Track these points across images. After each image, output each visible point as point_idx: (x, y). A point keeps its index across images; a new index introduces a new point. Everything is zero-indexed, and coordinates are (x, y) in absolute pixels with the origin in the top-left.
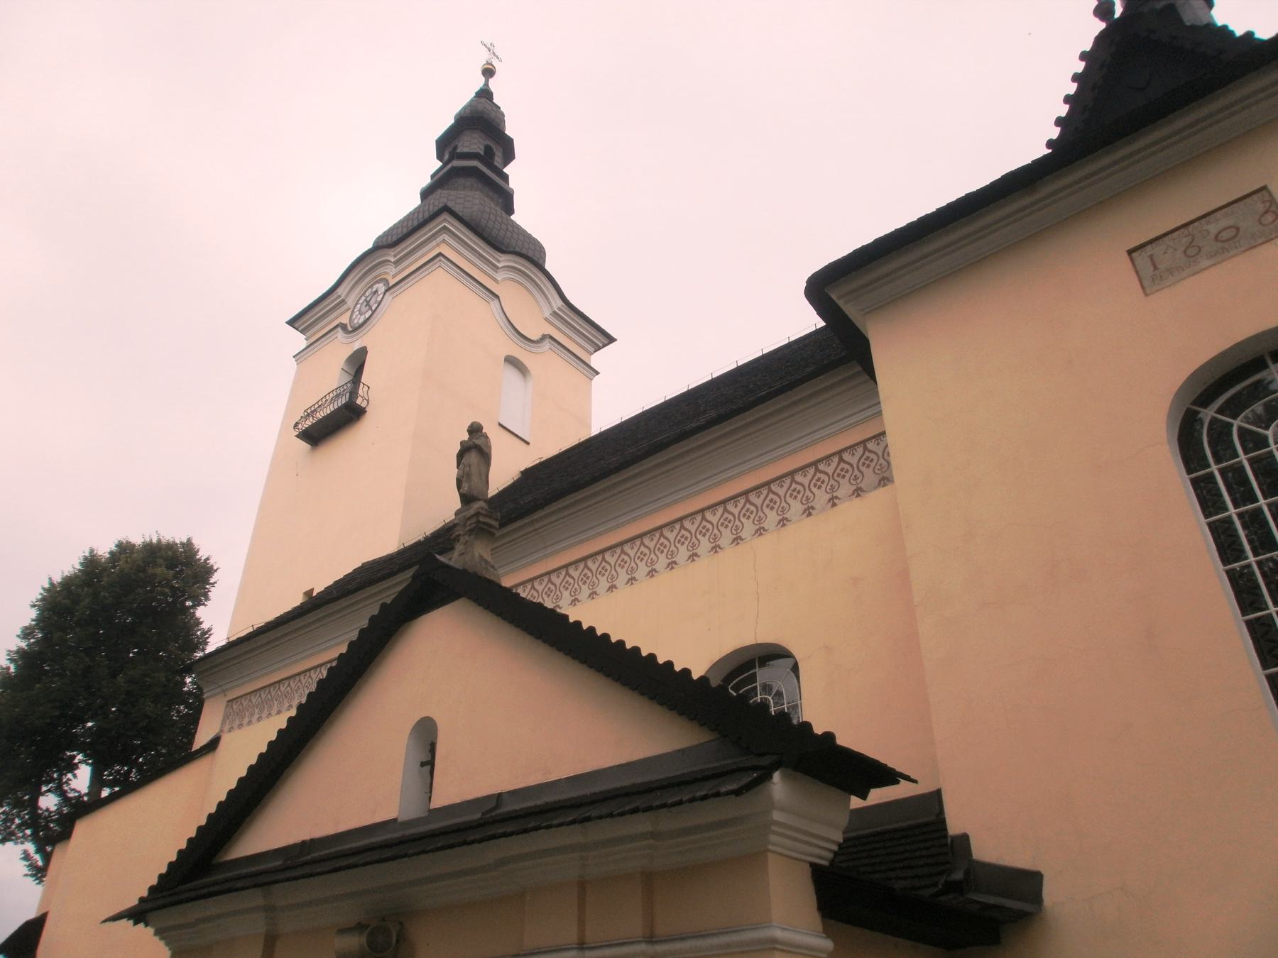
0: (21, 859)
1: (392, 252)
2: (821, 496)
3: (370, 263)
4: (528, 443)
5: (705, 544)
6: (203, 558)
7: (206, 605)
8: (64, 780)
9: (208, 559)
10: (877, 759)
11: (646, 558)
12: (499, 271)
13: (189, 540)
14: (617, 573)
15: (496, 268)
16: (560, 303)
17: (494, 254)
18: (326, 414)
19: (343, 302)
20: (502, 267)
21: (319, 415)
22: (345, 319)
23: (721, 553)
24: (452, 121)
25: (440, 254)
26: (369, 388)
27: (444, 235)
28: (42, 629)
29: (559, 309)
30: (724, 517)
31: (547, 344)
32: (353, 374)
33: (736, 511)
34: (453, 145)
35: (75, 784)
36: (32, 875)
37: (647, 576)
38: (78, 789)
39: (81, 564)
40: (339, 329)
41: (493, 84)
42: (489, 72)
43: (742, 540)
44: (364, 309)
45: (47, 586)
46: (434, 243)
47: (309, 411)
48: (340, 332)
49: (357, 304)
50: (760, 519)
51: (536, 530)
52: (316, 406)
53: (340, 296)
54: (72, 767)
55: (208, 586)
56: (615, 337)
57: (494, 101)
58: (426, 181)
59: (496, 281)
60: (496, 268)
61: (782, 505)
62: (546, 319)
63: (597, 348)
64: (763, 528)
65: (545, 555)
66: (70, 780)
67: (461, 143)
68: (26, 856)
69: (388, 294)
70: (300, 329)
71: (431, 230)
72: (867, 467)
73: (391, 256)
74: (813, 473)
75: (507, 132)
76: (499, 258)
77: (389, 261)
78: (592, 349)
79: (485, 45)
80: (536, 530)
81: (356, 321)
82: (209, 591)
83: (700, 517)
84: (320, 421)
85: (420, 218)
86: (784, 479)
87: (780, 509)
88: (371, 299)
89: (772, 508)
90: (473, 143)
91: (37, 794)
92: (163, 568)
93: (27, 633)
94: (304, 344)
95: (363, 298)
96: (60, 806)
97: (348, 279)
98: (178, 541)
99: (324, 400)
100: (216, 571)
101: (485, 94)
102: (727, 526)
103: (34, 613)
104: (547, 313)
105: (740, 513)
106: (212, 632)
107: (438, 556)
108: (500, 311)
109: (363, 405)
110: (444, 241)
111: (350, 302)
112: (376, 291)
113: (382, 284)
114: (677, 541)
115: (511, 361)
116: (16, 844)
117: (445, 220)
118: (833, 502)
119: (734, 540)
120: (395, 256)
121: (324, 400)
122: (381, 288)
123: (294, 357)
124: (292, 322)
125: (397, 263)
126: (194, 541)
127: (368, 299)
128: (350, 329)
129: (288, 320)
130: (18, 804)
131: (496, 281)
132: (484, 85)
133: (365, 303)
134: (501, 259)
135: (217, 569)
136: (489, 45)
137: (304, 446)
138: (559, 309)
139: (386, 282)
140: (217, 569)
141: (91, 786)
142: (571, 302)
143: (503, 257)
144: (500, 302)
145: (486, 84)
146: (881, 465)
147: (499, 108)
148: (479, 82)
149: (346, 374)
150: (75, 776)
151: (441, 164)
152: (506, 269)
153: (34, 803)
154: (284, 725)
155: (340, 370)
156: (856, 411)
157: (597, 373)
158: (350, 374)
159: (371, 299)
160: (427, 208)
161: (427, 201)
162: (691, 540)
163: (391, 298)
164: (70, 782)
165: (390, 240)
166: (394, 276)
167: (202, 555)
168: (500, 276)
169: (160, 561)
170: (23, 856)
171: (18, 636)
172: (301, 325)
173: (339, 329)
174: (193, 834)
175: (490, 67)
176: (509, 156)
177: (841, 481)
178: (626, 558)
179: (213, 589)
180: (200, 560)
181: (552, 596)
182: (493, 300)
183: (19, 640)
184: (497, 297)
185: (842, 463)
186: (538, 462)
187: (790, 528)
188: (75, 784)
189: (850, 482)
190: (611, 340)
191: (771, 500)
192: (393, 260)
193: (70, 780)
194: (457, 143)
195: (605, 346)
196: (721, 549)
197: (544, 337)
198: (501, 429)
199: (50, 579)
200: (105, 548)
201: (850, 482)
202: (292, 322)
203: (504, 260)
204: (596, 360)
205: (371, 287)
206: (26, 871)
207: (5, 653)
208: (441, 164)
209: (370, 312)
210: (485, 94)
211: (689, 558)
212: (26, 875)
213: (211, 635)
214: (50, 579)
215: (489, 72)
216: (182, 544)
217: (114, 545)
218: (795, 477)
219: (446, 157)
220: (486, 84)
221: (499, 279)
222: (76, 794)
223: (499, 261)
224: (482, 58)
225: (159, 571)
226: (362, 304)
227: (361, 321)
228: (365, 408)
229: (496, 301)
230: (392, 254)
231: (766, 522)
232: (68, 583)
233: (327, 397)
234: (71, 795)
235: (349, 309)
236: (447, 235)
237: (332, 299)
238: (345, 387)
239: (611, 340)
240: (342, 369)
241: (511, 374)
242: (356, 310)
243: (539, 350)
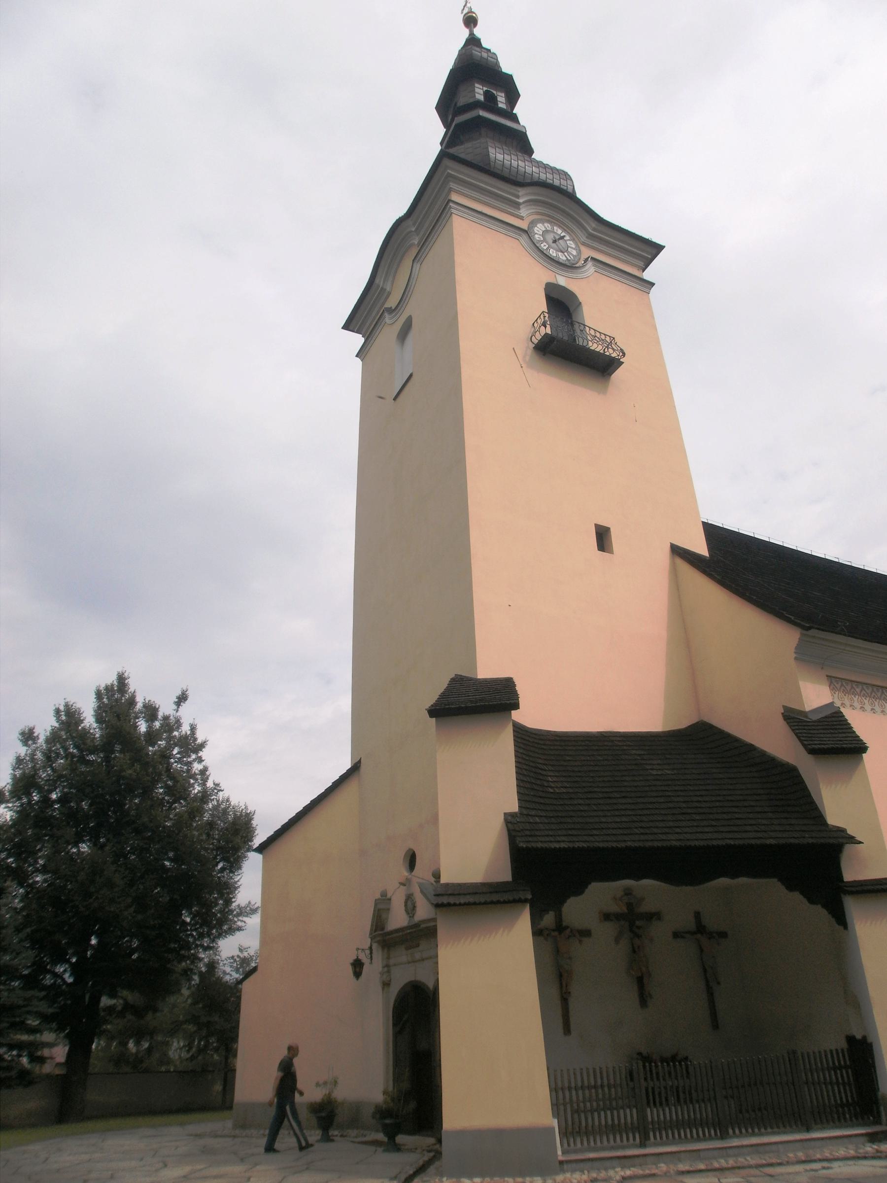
10: (395, 220)
12: (521, 207)
17: (512, 191)
20: (524, 202)
34: (453, 104)
41: (477, 32)
42: (470, 21)
48: (386, 314)
70: (355, 331)
75: (504, 70)
76: (517, 193)
77: (412, 231)
78: (641, 264)
94: (363, 340)
101: (473, 41)
107: (86, 1004)
120: (414, 224)
123: (357, 356)
132: (470, 35)
138: (594, 229)
142: (604, 218)
143: (521, 191)
144: (529, 235)
145: (472, 34)
148: (465, 33)
157: (653, 284)
163: (419, 265)
176: (513, 95)
203: (523, 195)
204: (648, 274)
210: (473, 41)
215: (470, 21)
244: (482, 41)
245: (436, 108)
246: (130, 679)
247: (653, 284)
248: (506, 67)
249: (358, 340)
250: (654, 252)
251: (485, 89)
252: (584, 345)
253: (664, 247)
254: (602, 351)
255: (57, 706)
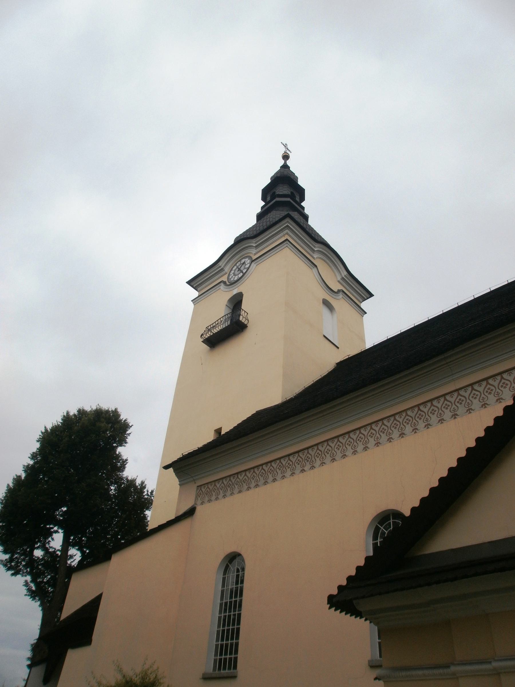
0: (23, 585)
1: (254, 241)
2: (448, 414)
3: (239, 248)
4: (338, 348)
5: (372, 442)
6: (123, 420)
7: (125, 446)
8: (47, 541)
9: (125, 420)
11: (374, 436)
13: (116, 409)
14: (368, 440)
15: (313, 251)
16: (345, 273)
17: (312, 243)
18: (222, 328)
19: (222, 270)
20: (316, 251)
21: (215, 331)
22: (225, 278)
23: (347, 459)
24: (269, 181)
25: (287, 240)
26: (247, 313)
27: (287, 230)
28: (40, 454)
29: (345, 276)
30: (394, 423)
31: (341, 295)
32: (232, 308)
33: (366, 433)
35: (52, 544)
36: (29, 595)
37: (363, 450)
38: (54, 547)
39: (62, 419)
40: (222, 284)
41: (289, 163)
42: (286, 157)
43: (347, 456)
44: (237, 273)
45: (44, 431)
46: (282, 234)
47: (209, 327)
48: (222, 286)
49: (232, 270)
50: (454, 410)
51: (447, 363)
52: (212, 326)
53: (220, 267)
54: (49, 534)
55: (125, 435)
56: (373, 294)
57: (290, 169)
58: (259, 210)
59: (314, 258)
60: (313, 251)
61: (401, 426)
62: (339, 281)
63: (364, 300)
64: (379, 443)
65: (453, 379)
66: (50, 541)
67: (278, 190)
68: (26, 584)
69: (253, 263)
71: (280, 227)
72: (350, 441)
73: (253, 243)
74: (485, 385)
77: (253, 246)
78: (361, 300)
79: (283, 144)
80: (447, 363)
81: (232, 279)
82: (127, 438)
83: (393, 418)
84: (214, 334)
85: (264, 225)
86: (453, 393)
87: (400, 428)
88: (241, 267)
89: (372, 437)
90: (283, 190)
91: (33, 549)
92: (105, 423)
93: (34, 456)
95: (235, 267)
96: (44, 556)
97: (223, 260)
98: (110, 410)
99: (219, 321)
100: (131, 426)
101: (285, 167)
102: (361, 441)
103: (38, 445)
104: (339, 278)
105: (391, 426)
106: (127, 462)
108: (318, 274)
109: (246, 323)
110: (287, 234)
111: (227, 269)
112: (244, 263)
113: (247, 259)
114: (380, 431)
115: (326, 303)
116: (22, 576)
117: (288, 222)
118: (428, 427)
119: (400, 435)
121: (219, 321)
122: (248, 261)
123: (192, 301)
124: (189, 283)
125: (257, 247)
126: (119, 410)
127: (239, 267)
128: (228, 283)
129: (187, 281)
130: (25, 554)
131: (314, 258)
133: (237, 269)
134: (316, 246)
135: (132, 425)
136: (285, 144)
137: (205, 347)
138: (345, 276)
139: (250, 257)
140: (132, 425)
141: (63, 546)
143: (317, 245)
145: (285, 163)
146: (468, 403)
147: (295, 174)
148: (282, 162)
149: (228, 308)
150: (53, 539)
151: (264, 203)
152: (318, 252)
153: (32, 552)
154: (500, 413)
155: (225, 305)
156: (511, 350)
157: (366, 313)
158: (230, 308)
159: (241, 267)
160: (261, 224)
161: (261, 221)
162: (354, 443)
163: (255, 265)
164: (50, 543)
165: (252, 234)
166: (255, 254)
167: (123, 417)
168: (315, 256)
169: (103, 420)
170: (24, 584)
171: (29, 457)
172: (195, 284)
173: (222, 284)
174: (426, 494)
175: (287, 154)
177: (407, 426)
178: (374, 432)
179: (129, 437)
180: (121, 420)
181: (351, 445)
182: (314, 268)
183: (30, 459)
184: (316, 266)
185: (488, 385)
186: (347, 357)
187: (369, 451)
188: (52, 544)
189: (465, 406)
190: (371, 295)
191: (446, 405)
192: (254, 245)
193: (50, 541)
194: (275, 191)
195: (368, 298)
196: (369, 448)
197: (339, 291)
198: (325, 339)
199: (45, 427)
200: (73, 411)
201: (465, 406)
202: (189, 283)
203: (317, 247)
204: (364, 305)
205: (240, 261)
206: (25, 592)
207: (22, 467)
208: (264, 203)
209: (241, 274)
210: (285, 167)
211: (255, 486)
212: (26, 595)
213: (127, 463)
214: (45, 427)
215: (286, 157)
216: (112, 411)
217: (76, 411)
218: (489, 381)
219: (269, 199)
220: (285, 163)
221: (315, 257)
222: (53, 550)
223: (315, 247)
224: (282, 150)
225: (103, 425)
226: (235, 270)
227: (236, 279)
228: (246, 324)
229: (315, 269)
230: (254, 242)
231: (286, 474)
232: (55, 429)
233: (222, 319)
234: (51, 550)
235: (226, 273)
236: (289, 230)
237: (205, 275)
238: (222, 319)
239: (371, 295)
240: (226, 305)
241: (325, 311)
242: (231, 274)
243: (338, 298)
244: (290, 168)
245: (304, 190)
246: (103, 407)
247: (366, 313)
248: (301, 182)
249: (195, 294)
250: (368, 296)
251: (291, 191)
252: (220, 329)
253: (374, 295)
254: (212, 334)
255: (79, 408)
